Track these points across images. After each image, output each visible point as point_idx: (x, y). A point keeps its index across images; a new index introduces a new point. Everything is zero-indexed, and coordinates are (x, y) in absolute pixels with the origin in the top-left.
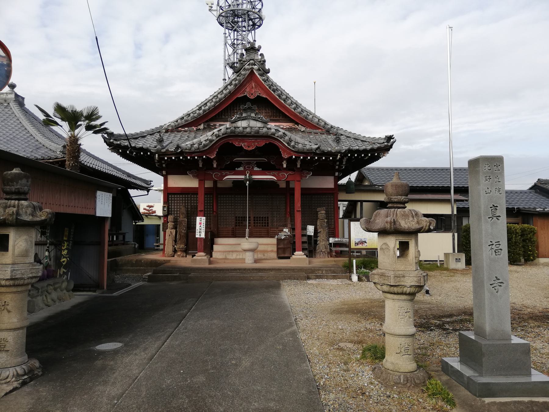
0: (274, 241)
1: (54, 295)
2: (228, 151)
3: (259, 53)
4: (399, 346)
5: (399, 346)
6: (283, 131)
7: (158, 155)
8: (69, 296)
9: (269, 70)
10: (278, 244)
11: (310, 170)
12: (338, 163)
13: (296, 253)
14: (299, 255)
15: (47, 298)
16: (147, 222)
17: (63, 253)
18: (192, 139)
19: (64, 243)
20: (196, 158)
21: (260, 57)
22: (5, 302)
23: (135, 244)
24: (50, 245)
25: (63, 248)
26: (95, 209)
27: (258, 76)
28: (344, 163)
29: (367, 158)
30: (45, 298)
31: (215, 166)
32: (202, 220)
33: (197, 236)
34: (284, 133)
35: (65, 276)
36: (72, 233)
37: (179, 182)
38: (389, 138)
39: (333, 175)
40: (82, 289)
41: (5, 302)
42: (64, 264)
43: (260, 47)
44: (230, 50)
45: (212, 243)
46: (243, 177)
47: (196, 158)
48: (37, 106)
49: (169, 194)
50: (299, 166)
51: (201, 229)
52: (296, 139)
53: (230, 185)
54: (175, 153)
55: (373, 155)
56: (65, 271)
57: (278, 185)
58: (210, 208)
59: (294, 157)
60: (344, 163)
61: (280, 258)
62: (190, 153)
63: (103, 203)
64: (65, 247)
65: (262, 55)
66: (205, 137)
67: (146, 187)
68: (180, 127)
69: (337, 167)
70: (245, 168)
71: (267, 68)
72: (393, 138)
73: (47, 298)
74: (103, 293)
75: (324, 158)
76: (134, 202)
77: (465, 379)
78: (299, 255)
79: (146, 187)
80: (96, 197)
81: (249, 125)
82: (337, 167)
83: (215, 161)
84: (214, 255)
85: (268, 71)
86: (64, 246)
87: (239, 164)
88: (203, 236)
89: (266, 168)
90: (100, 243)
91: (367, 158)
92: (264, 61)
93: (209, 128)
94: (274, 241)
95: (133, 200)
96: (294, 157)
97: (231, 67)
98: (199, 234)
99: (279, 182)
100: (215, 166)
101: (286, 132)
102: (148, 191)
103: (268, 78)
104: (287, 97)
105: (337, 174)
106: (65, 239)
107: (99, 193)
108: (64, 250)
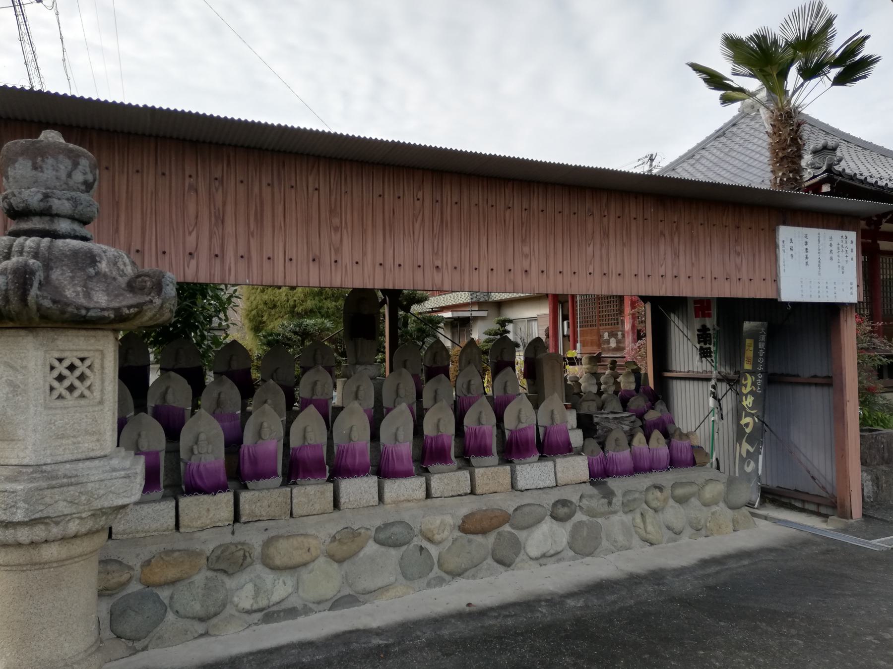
1: (674, 514)
8: (735, 522)
15: (644, 522)
17: (744, 403)
19: (746, 379)
24: (718, 380)
25: (745, 391)
26: (776, 280)
30: (638, 520)
35: (752, 464)
36: (761, 353)
40: (812, 507)
42: (748, 430)
48: (697, 68)
56: (752, 450)
63: (813, 261)
64: (749, 389)
73: (644, 522)
74: (845, 531)
77: (752, 45)
80: (776, 246)
86: (746, 386)
90: (830, 382)
106: (748, 366)
107: (785, 233)
108: (746, 395)
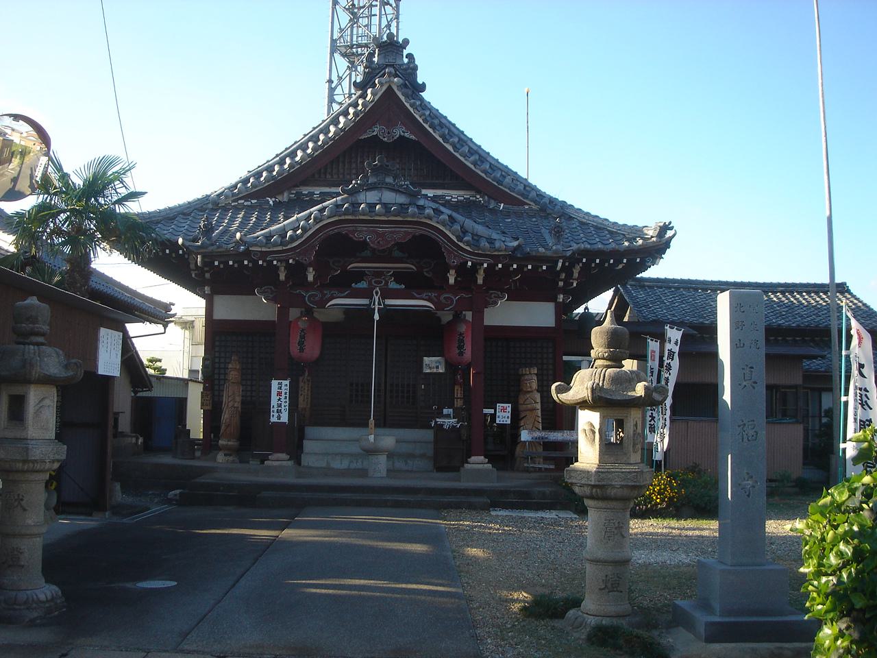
0: (428, 435)
2: (336, 249)
3: (405, 52)
4: (604, 578)
5: (604, 578)
6: (449, 212)
7: (203, 258)
9: (423, 83)
10: (436, 441)
11: (502, 291)
12: (563, 276)
13: (473, 459)
14: (478, 462)
16: (157, 392)
18: (269, 225)
20: (275, 262)
21: (406, 60)
22: (19, 495)
23: (137, 439)
27: (403, 98)
28: (576, 275)
29: (620, 266)
31: (310, 278)
32: (283, 387)
33: (274, 419)
34: (450, 216)
37: (234, 308)
38: (665, 228)
39: (553, 299)
41: (19, 495)
43: (406, 42)
44: (345, 18)
45: (302, 437)
46: (365, 301)
47: (275, 262)
49: (219, 336)
50: (480, 281)
51: (280, 406)
52: (473, 229)
53: (338, 316)
54: (239, 257)
55: (631, 262)
57: (439, 319)
58: (219, 368)
59: (470, 263)
60: (576, 275)
61: (440, 469)
62: (263, 255)
65: (410, 56)
66: (293, 224)
67: (159, 314)
68: (240, 199)
69: (561, 284)
70: (370, 283)
71: (420, 81)
72: (672, 228)
75: (530, 267)
76: (135, 348)
78: (478, 462)
79: (159, 314)
81: (380, 199)
82: (561, 284)
83: (311, 269)
84: (306, 460)
85: (423, 87)
87: (359, 276)
88: (285, 418)
89: (412, 284)
91: (620, 266)
92: (416, 68)
93: (302, 203)
94: (428, 435)
95: (133, 344)
96: (470, 263)
97: (344, 55)
98: (276, 415)
99: (439, 313)
100: (310, 278)
101: (455, 215)
102: (165, 327)
103: (422, 99)
104: (460, 139)
105: (561, 298)
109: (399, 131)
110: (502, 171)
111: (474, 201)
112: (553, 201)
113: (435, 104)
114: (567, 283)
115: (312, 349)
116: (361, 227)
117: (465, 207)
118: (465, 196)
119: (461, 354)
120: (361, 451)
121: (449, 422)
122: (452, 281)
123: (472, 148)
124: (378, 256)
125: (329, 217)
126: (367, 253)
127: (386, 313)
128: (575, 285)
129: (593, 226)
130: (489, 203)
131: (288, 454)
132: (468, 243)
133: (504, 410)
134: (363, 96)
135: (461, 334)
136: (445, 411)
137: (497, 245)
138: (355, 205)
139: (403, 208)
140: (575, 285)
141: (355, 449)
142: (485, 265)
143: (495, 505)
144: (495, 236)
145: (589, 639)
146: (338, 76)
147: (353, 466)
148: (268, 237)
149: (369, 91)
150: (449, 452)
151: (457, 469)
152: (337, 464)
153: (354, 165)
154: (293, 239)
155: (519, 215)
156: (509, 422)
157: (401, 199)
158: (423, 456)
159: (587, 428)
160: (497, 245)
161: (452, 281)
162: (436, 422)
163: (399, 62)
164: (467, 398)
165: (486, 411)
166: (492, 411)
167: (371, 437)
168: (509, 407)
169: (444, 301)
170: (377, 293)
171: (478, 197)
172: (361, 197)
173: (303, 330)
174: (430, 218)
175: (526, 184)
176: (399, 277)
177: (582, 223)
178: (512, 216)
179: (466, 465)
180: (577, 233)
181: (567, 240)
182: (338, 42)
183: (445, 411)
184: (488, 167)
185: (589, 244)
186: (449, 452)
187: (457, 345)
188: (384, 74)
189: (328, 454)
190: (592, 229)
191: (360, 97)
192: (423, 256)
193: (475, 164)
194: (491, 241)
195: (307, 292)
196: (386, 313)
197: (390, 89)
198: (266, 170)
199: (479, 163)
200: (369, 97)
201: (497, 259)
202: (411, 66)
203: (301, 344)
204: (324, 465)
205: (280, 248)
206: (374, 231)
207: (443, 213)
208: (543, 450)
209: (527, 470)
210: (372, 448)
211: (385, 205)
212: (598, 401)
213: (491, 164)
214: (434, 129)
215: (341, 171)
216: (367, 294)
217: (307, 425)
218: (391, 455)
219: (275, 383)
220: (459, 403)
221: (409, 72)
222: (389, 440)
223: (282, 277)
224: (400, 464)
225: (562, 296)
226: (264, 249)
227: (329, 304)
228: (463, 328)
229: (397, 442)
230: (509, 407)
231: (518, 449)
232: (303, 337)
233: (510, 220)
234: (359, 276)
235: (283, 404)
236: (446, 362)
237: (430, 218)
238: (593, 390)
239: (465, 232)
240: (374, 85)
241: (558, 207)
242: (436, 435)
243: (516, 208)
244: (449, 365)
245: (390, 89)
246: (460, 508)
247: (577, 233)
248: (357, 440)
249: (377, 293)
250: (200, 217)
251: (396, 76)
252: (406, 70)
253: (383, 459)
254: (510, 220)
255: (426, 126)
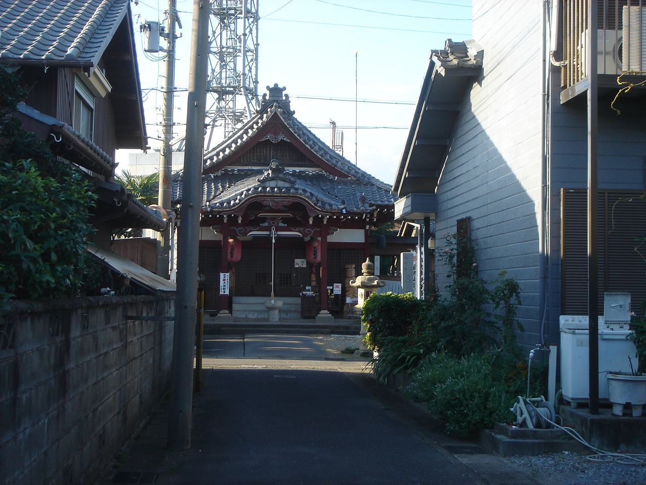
0: (298, 300)
3: (284, 93)
9: (294, 111)
13: (322, 312)
14: (324, 313)
28: (375, 215)
31: (240, 221)
33: (222, 293)
39: (364, 228)
43: (284, 89)
46: (267, 233)
51: (225, 286)
60: (375, 215)
61: (305, 317)
62: (219, 212)
65: (287, 96)
78: (324, 313)
81: (277, 185)
85: (294, 112)
87: (264, 220)
89: (291, 224)
94: (298, 300)
98: (223, 291)
105: (368, 227)
109: (281, 137)
110: (336, 159)
111: (321, 174)
112: (364, 174)
113: (300, 120)
114: (371, 219)
115: (237, 256)
116: (268, 199)
117: (315, 180)
118: (316, 171)
119: (315, 258)
120: (265, 309)
121: (310, 293)
122: (311, 222)
123: (320, 147)
124: (272, 210)
125: (252, 194)
126: (266, 209)
127: (278, 238)
128: (375, 220)
129: (384, 190)
130: (330, 176)
131: (228, 310)
132: (319, 207)
133: (337, 287)
134: (261, 118)
135: (315, 248)
136: (307, 288)
137: (334, 207)
138: (264, 188)
139: (288, 189)
140: (375, 220)
141: (262, 308)
142: (328, 217)
143: (333, 333)
144: (332, 202)
145: (361, 356)
146: (213, 31)
147: (260, 317)
148: (222, 203)
149: (265, 115)
150: (309, 309)
151: (314, 318)
152: (251, 316)
153: (255, 154)
154: (234, 205)
155: (345, 183)
156: (340, 293)
157: (287, 185)
158: (295, 311)
159: (361, 294)
160: (334, 207)
161: (311, 222)
162: (303, 294)
163: (280, 99)
164: (318, 279)
165: (328, 287)
166: (331, 288)
167: (273, 301)
168: (340, 285)
169: (307, 232)
170: (273, 229)
171: (323, 172)
172: (267, 184)
173: (232, 246)
174: (301, 194)
175: (349, 165)
176: (284, 220)
177: (379, 188)
178: (342, 184)
179: (318, 315)
180: (375, 195)
181: (369, 199)
182: (213, 5)
183: (307, 288)
184: (329, 157)
185: (381, 201)
186: (309, 309)
187: (313, 253)
188: (272, 106)
189: (245, 311)
190: (384, 191)
191: (259, 118)
192: (297, 212)
193: (322, 155)
194: (331, 205)
195: (237, 228)
196: (278, 238)
197: (276, 113)
198: (209, 159)
199: (324, 155)
200: (265, 119)
201: (334, 214)
202: (287, 101)
203: (231, 253)
204: (244, 317)
205: (228, 209)
206: (273, 201)
207: (307, 191)
208: (201, 242)
209: (350, 318)
210: (276, 306)
211: (280, 189)
212: (363, 286)
213: (330, 155)
214: (300, 137)
215: (249, 157)
216: (268, 229)
217: (234, 296)
218: (281, 311)
219: (222, 275)
220: (314, 283)
221: (285, 105)
222: (279, 302)
223: (225, 221)
224: (283, 316)
225: (368, 226)
226: (220, 210)
227: (249, 234)
228: (316, 244)
229: (284, 304)
230: (340, 285)
231: (345, 308)
232: (232, 250)
233: (340, 187)
234: (264, 220)
235: (226, 283)
236: (307, 262)
237: (301, 194)
238: (361, 283)
239: (318, 201)
240: (267, 113)
241: (366, 179)
242: (302, 301)
243: (343, 179)
244: (308, 263)
245: (276, 113)
246: (317, 333)
247: (375, 195)
248: (264, 304)
249: (273, 229)
250: (176, 186)
251: (280, 107)
252: (284, 103)
253: (277, 312)
254: (340, 187)
255: (296, 135)
